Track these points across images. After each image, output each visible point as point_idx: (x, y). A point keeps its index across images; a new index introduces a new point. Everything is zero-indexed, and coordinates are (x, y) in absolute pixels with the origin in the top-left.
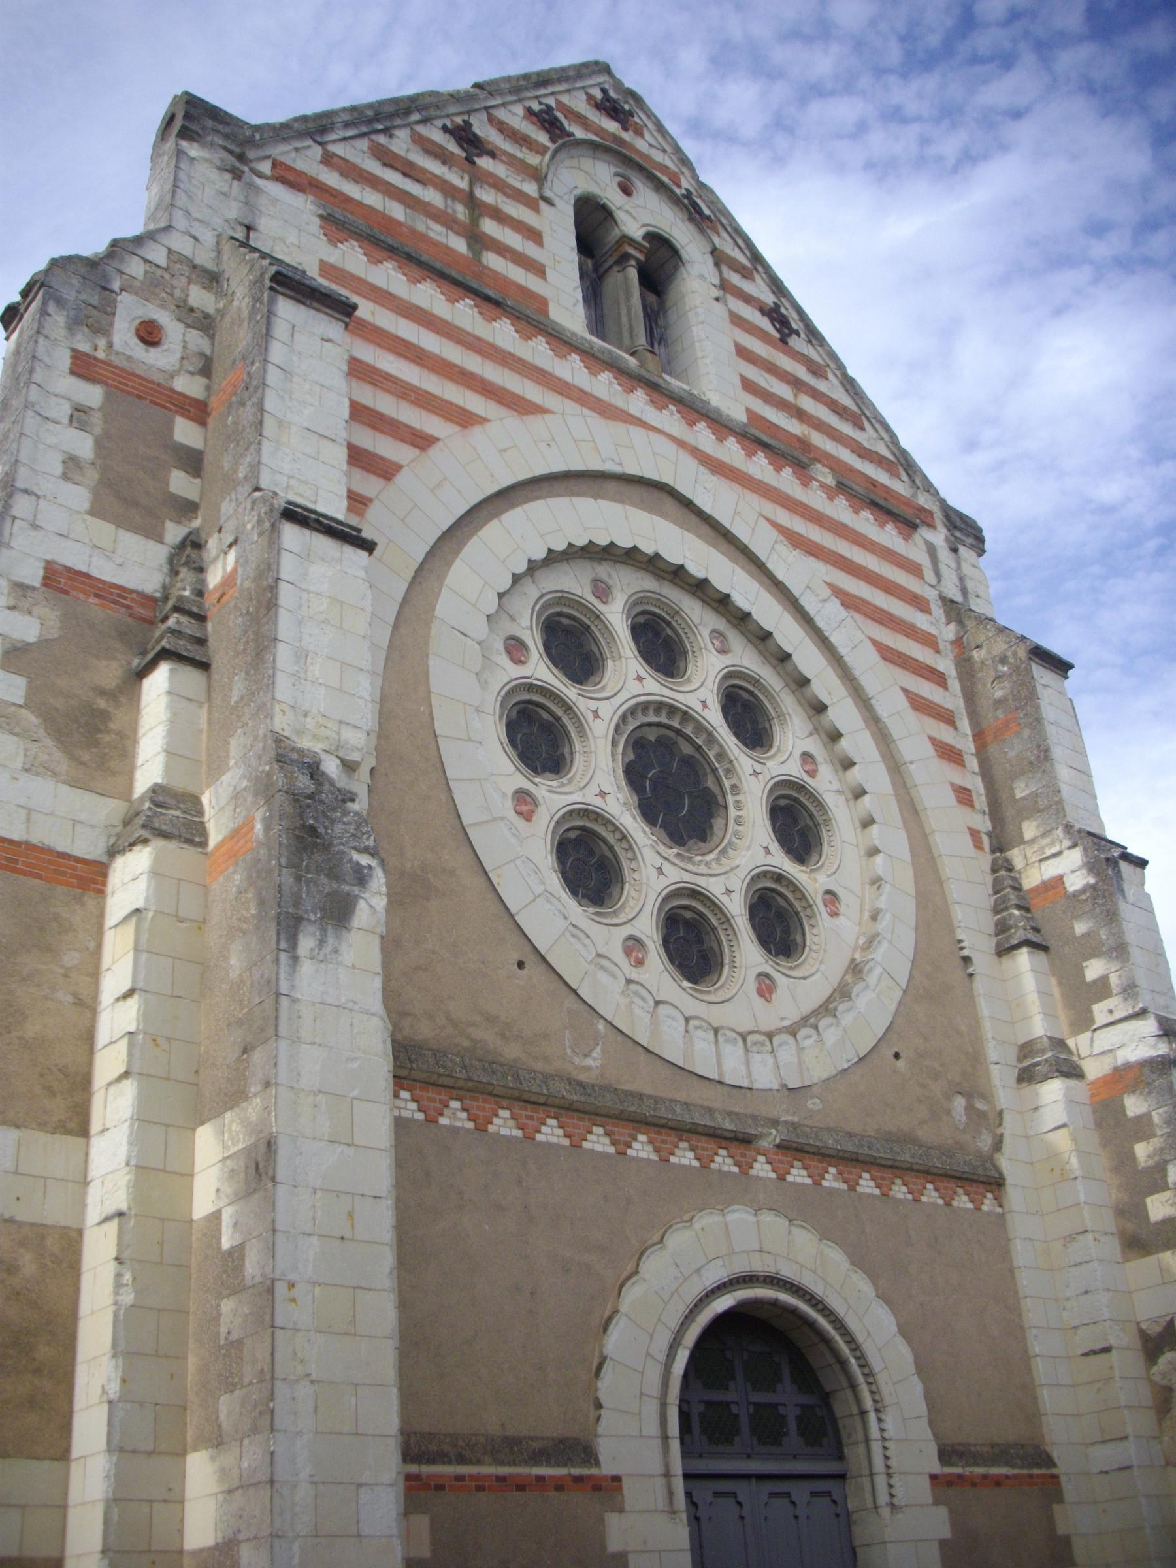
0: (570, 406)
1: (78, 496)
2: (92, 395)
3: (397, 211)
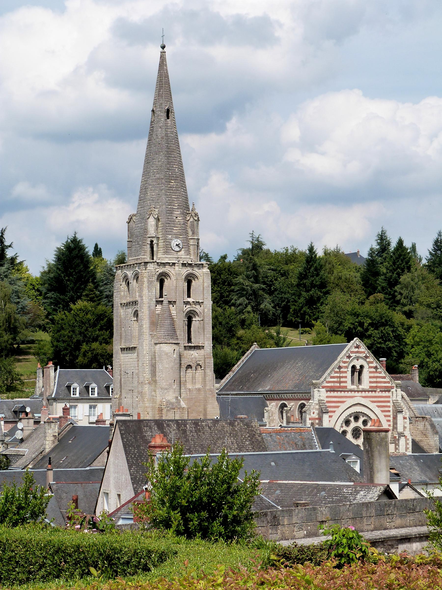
3: (332, 384)
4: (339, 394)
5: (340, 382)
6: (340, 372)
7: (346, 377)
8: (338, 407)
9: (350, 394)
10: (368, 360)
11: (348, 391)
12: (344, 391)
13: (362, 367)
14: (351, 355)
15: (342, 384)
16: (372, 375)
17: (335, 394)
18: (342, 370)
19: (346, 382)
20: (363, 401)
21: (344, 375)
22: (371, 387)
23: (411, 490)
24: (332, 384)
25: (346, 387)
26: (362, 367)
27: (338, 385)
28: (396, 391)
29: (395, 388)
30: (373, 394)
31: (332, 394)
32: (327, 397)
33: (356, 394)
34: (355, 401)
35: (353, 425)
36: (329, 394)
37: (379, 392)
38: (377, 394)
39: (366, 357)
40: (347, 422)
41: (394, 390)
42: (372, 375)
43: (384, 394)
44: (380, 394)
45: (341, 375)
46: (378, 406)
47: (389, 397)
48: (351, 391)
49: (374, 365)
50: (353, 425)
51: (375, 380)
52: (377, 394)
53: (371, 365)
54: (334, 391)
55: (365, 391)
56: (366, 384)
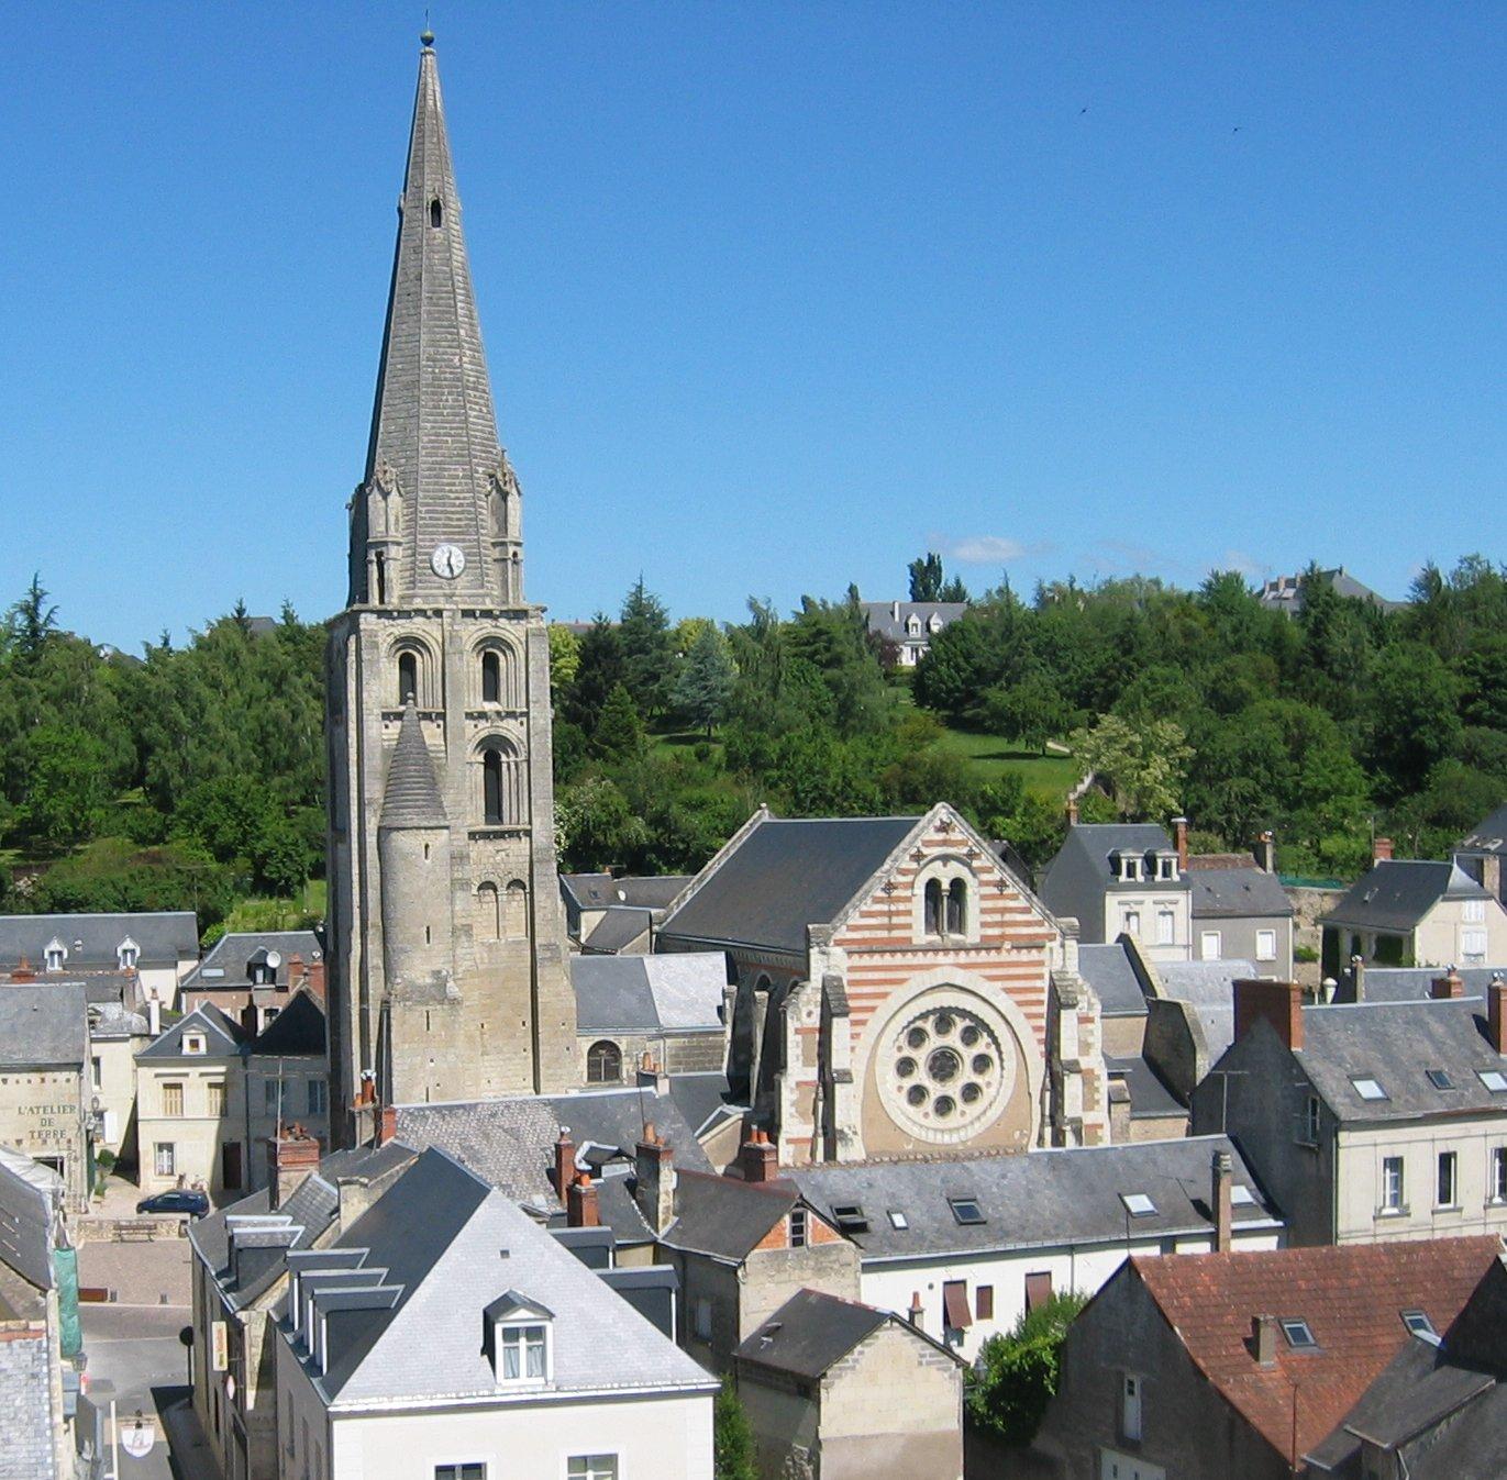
0: (917, 973)
1: (800, 1063)
2: (799, 1038)
4: (887, 959)
5: (890, 927)
6: (891, 900)
7: (909, 913)
8: (884, 995)
9: (920, 959)
10: (975, 864)
11: (914, 951)
12: (904, 952)
13: (958, 885)
14: (925, 851)
15: (896, 934)
16: (989, 904)
17: (877, 960)
18: (895, 893)
19: (908, 926)
20: (960, 977)
21: (908, 906)
22: (984, 938)
23: (904, 1335)
24: (867, 934)
25: (909, 940)
26: (958, 885)
27: (884, 934)
28: (1063, 946)
29: (1058, 938)
30: (993, 956)
31: (866, 960)
32: (851, 969)
33: (941, 958)
34: (920, 981)
35: (934, 1041)
36: (856, 960)
37: (1008, 951)
38: (1004, 957)
39: (972, 855)
40: (917, 1037)
41: (1056, 944)
42: (989, 904)
43: (1024, 956)
44: (1015, 956)
45: (893, 908)
46: (1008, 991)
47: (1041, 963)
48: (925, 951)
49: (996, 875)
50: (934, 1041)
51: (997, 917)
52: (1004, 957)
53: (985, 877)
54: (871, 952)
55: (967, 950)
56: (973, 933)
